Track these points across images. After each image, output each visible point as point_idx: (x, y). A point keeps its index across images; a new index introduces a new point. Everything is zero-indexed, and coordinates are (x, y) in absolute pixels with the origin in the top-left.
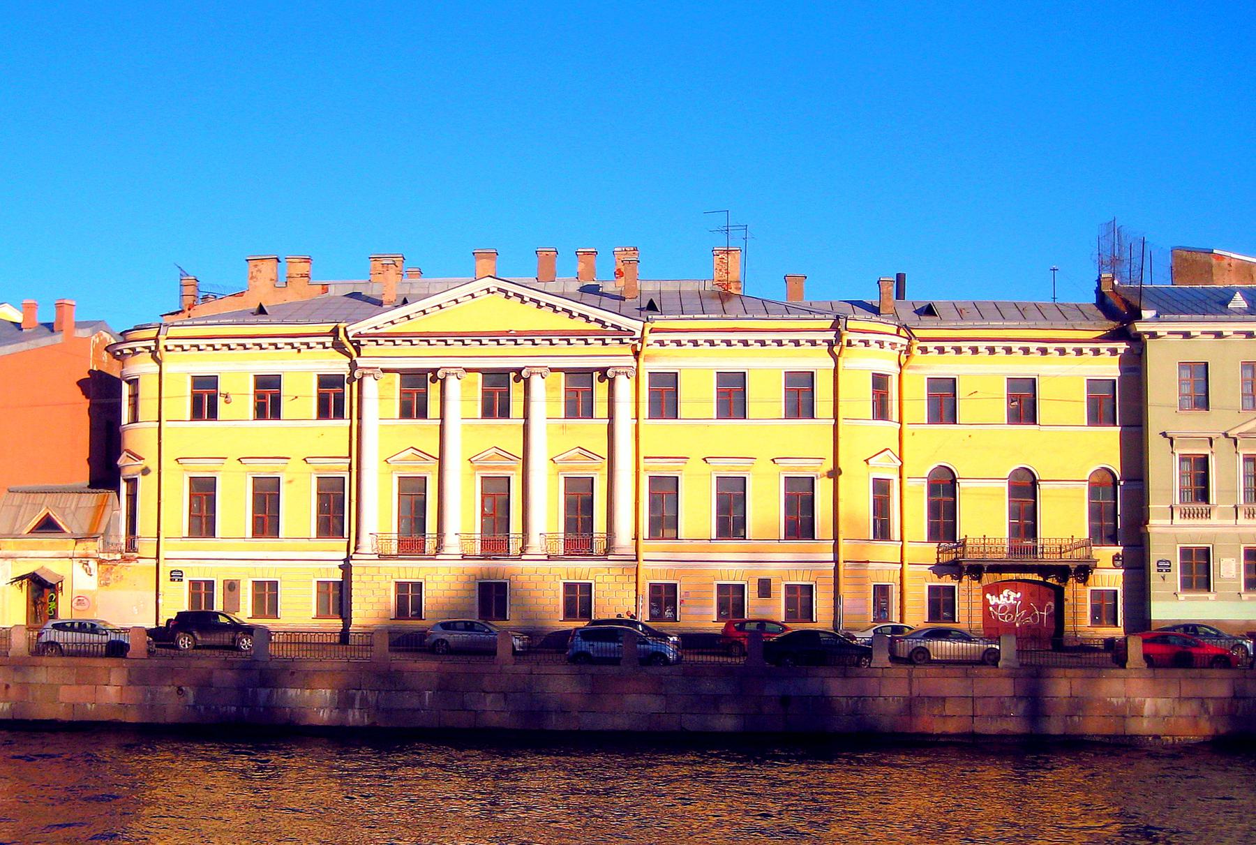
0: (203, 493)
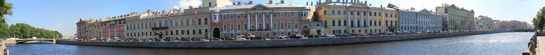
0: (334, 22)
